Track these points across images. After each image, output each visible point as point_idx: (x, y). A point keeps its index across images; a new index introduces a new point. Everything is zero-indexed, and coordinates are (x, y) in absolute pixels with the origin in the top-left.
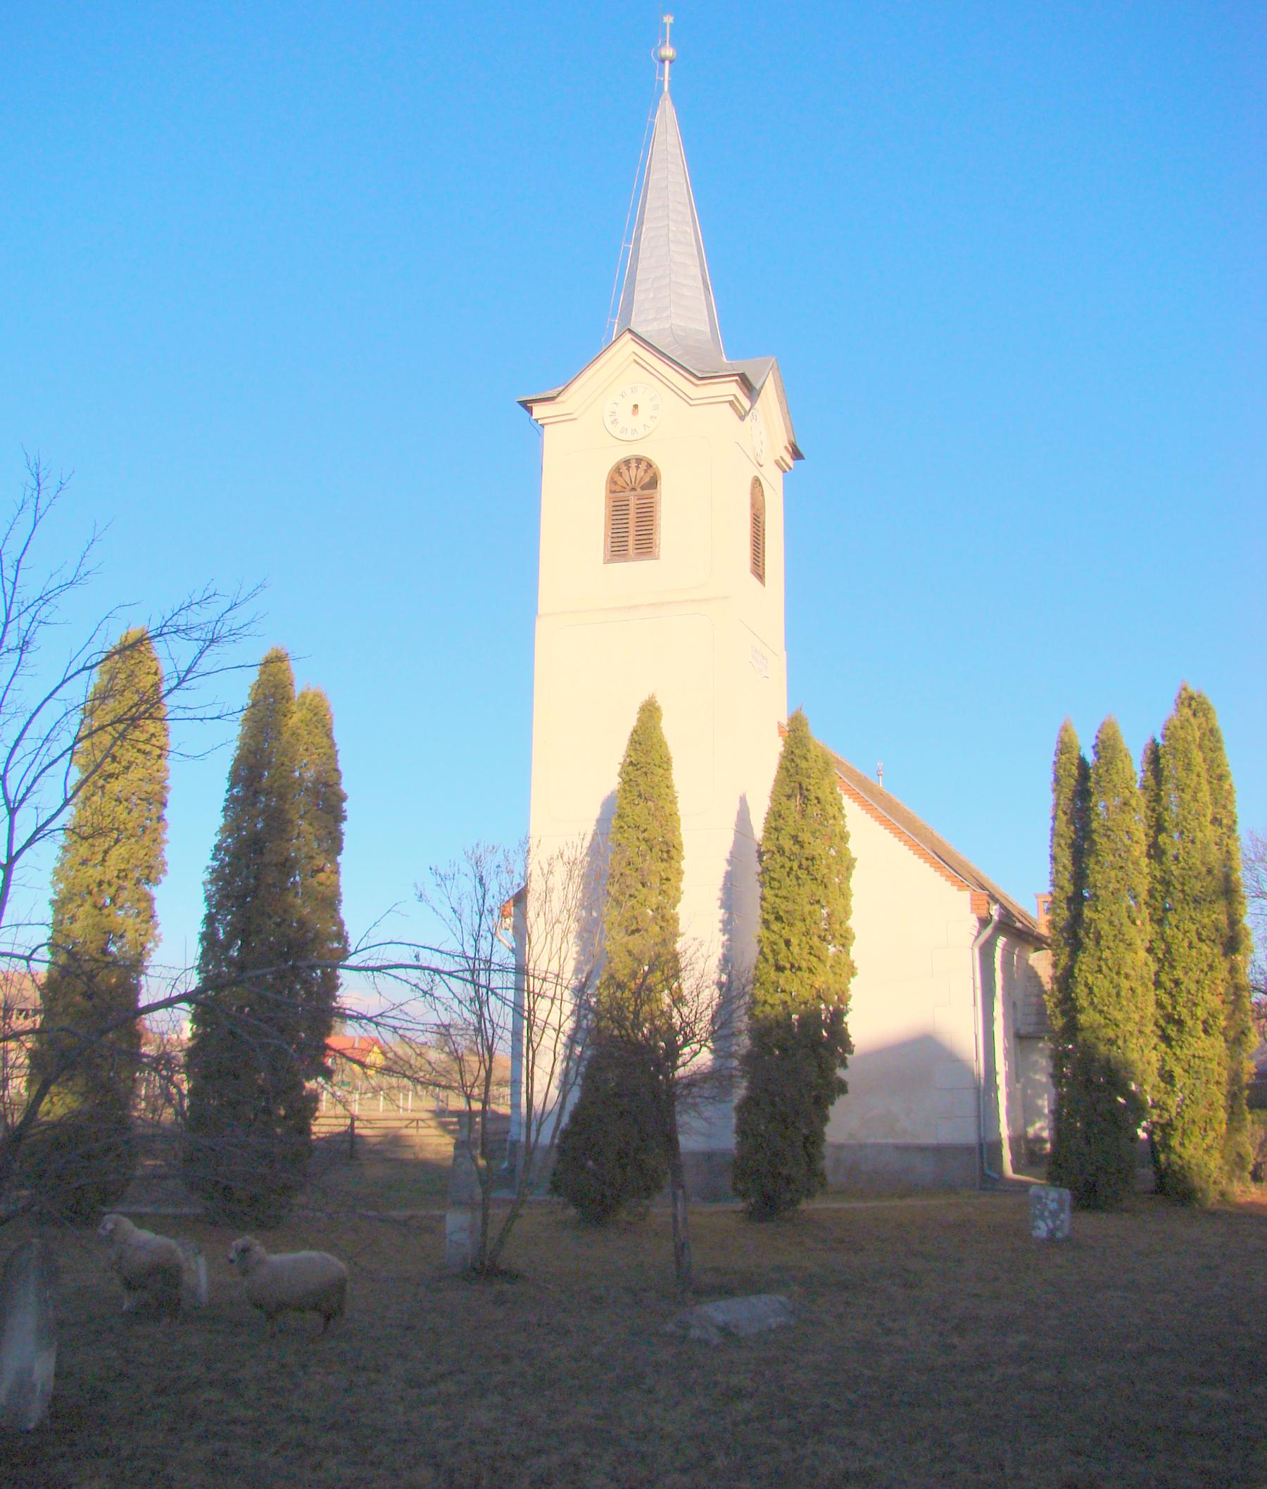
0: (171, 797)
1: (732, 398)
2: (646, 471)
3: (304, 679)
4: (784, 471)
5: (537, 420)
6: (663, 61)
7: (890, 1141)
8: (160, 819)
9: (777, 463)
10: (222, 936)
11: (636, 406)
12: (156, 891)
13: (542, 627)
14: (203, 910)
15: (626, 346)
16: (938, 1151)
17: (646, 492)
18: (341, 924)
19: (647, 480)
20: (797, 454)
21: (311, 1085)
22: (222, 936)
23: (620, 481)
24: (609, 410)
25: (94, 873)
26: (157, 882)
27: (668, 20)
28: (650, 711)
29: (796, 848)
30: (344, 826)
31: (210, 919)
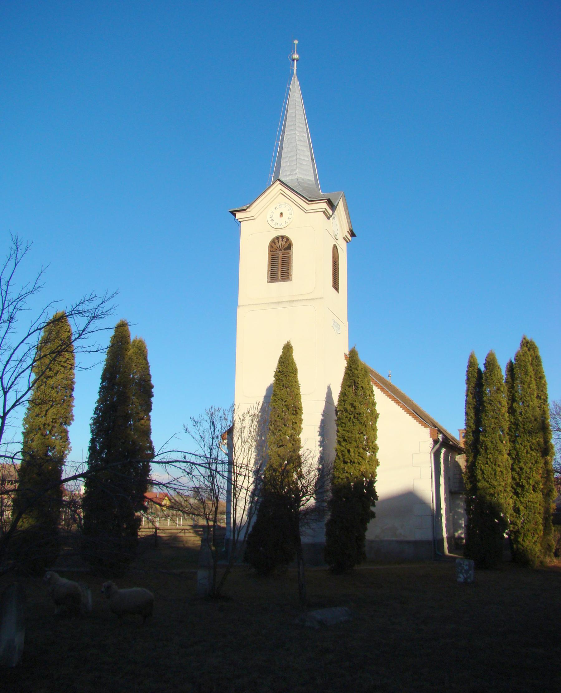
0: (76, 386)
1: (324, 210)
2: (286, 242)
3: (134, 334)
4: (347, 242)
5: (238, 219)
6: (293, 60)
7: (394, 539)
8: (71, 396)
9: (344, 238)
10: (98, 448)
11: (281, 213)
12: (69, 428)
13: (240, 311)
14: (90, 436)
15: (277, 187)
16: (416, 543)
17: (286, 251)
18: (151, 443)
19: (286, 246)
20: (353, 234)
21: (138, 514)
22: (98, 448)
23: (274, 246)
24: (270, 214)
25: (42, 420)
26: (70, 424)
27: (296, 42)
28: (288, 349)
29: (352, 409)
30: (153, 400)
31: (93, 441)
